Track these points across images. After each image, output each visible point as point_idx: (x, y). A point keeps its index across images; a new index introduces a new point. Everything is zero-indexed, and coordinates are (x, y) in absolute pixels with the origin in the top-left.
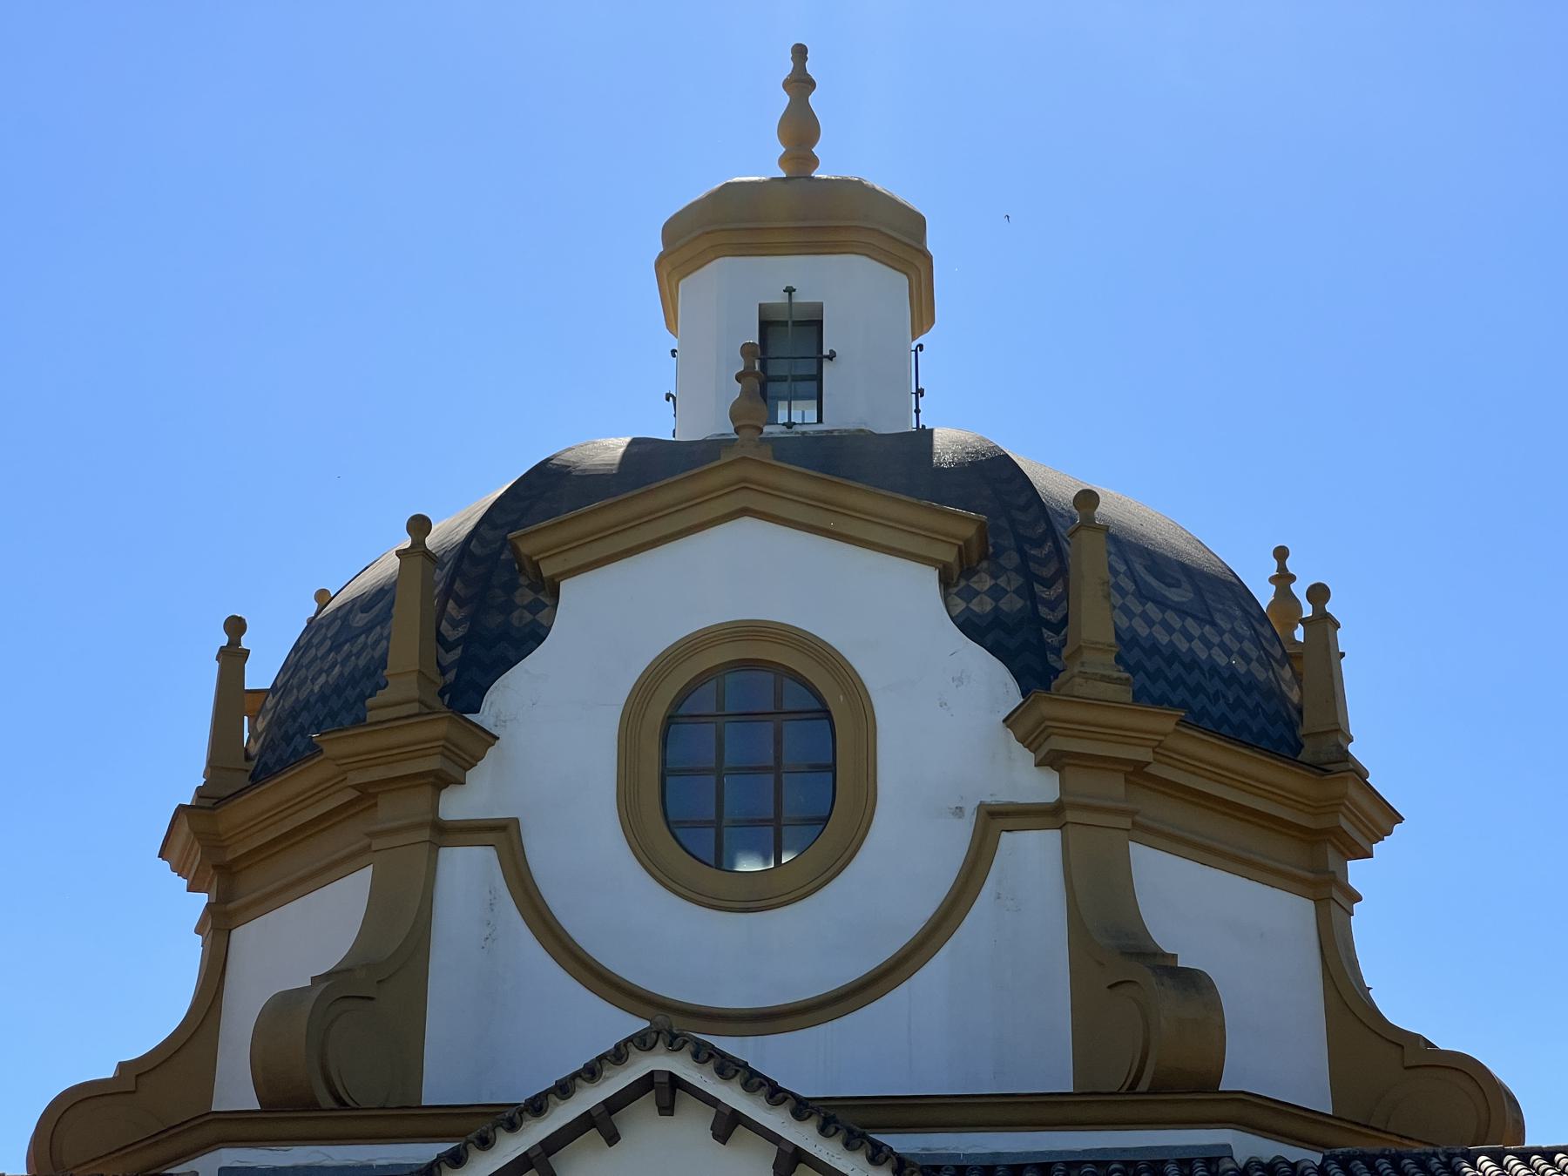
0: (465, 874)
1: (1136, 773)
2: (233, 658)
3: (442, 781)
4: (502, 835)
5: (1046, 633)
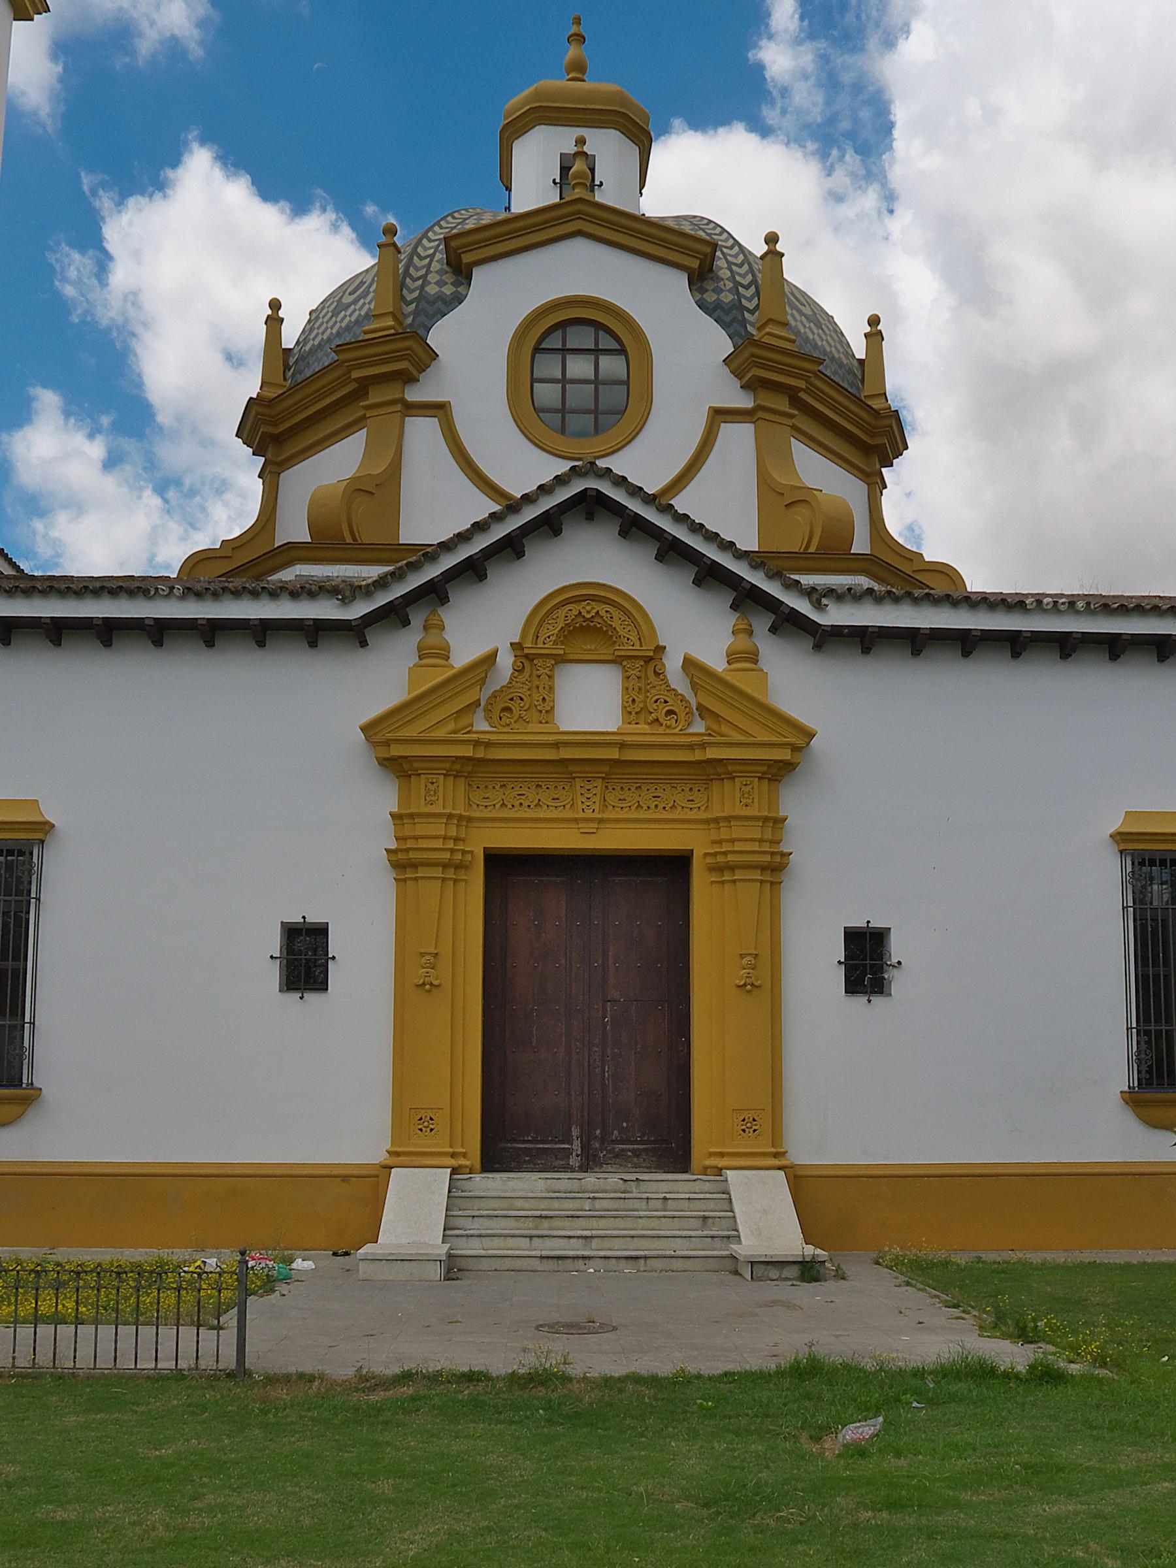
0: (422, 434)
1: (796, 401)
2: (274, 322)
3: (409, 379)
4: (439, 410)
5: (746, 314)
